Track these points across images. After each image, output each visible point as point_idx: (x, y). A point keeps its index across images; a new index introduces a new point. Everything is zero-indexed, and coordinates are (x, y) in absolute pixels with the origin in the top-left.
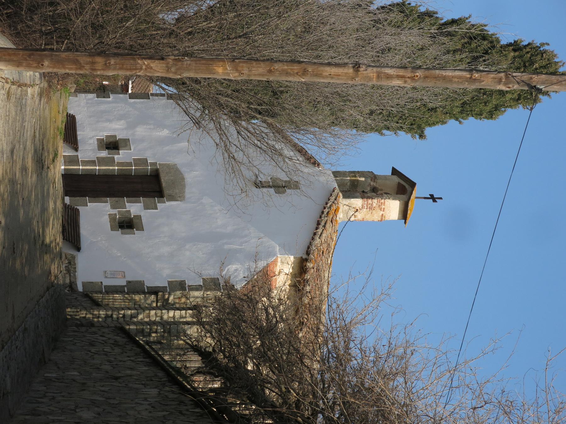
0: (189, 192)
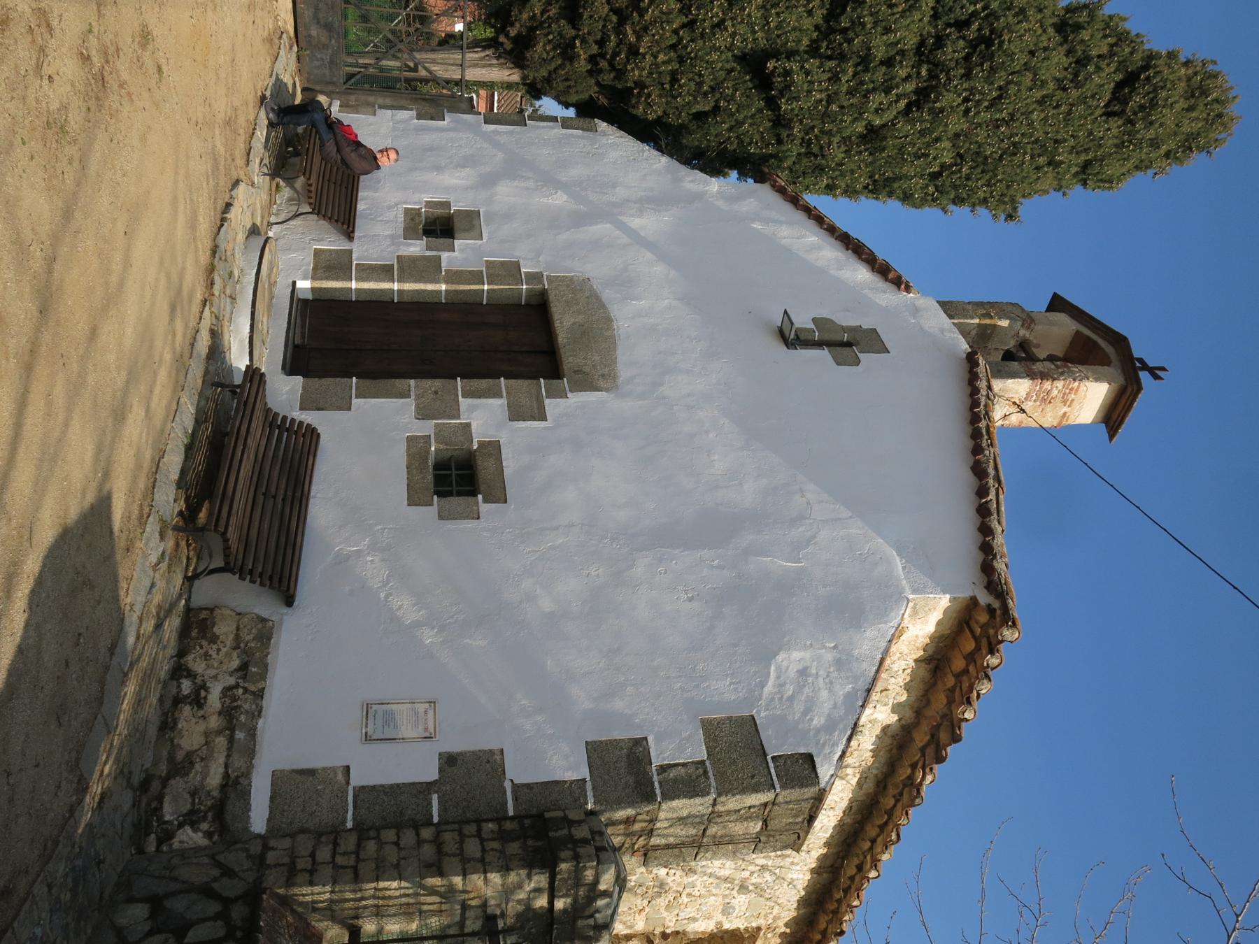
0: (632, 357)
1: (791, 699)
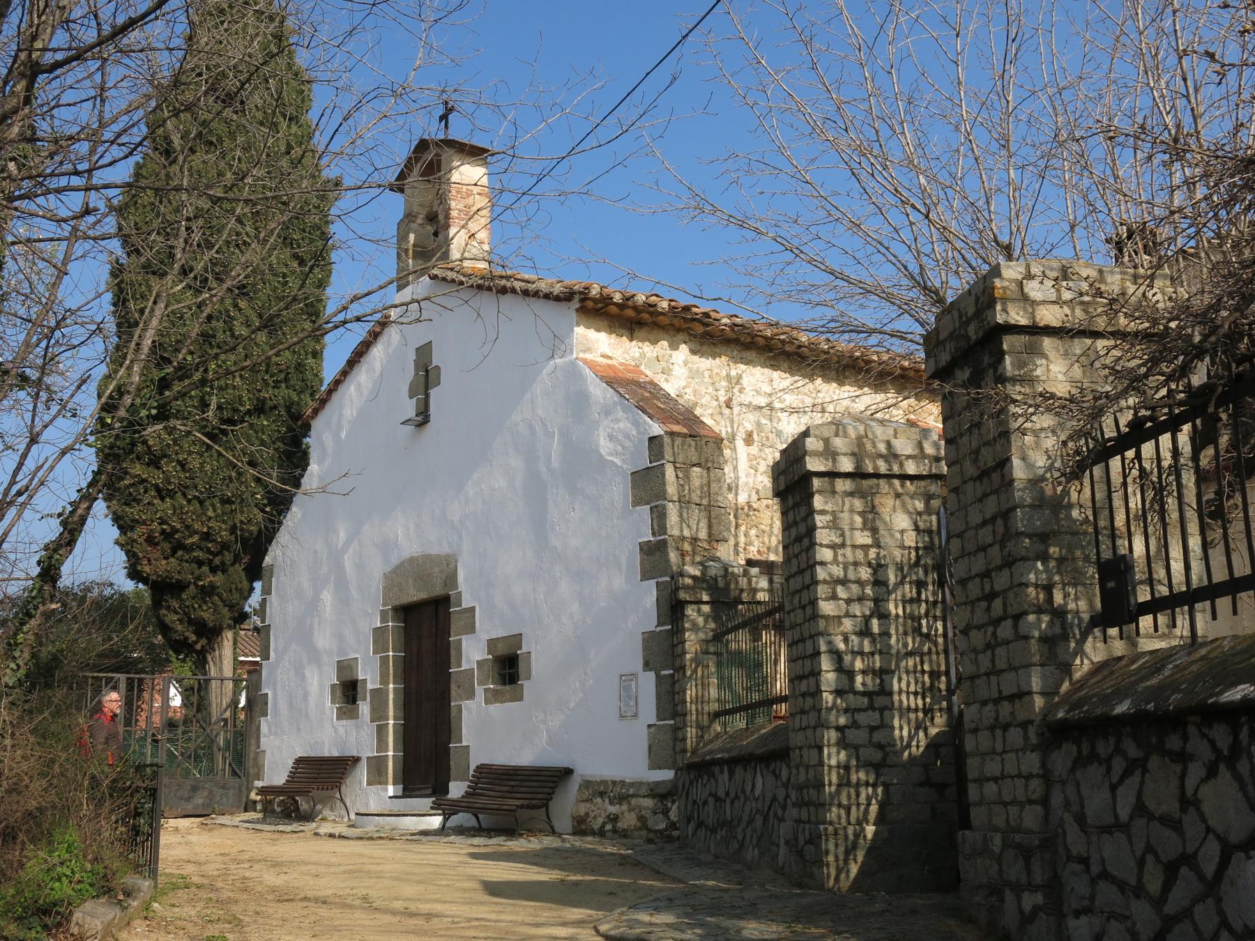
0: (437, 546)
1: (623, 448)
